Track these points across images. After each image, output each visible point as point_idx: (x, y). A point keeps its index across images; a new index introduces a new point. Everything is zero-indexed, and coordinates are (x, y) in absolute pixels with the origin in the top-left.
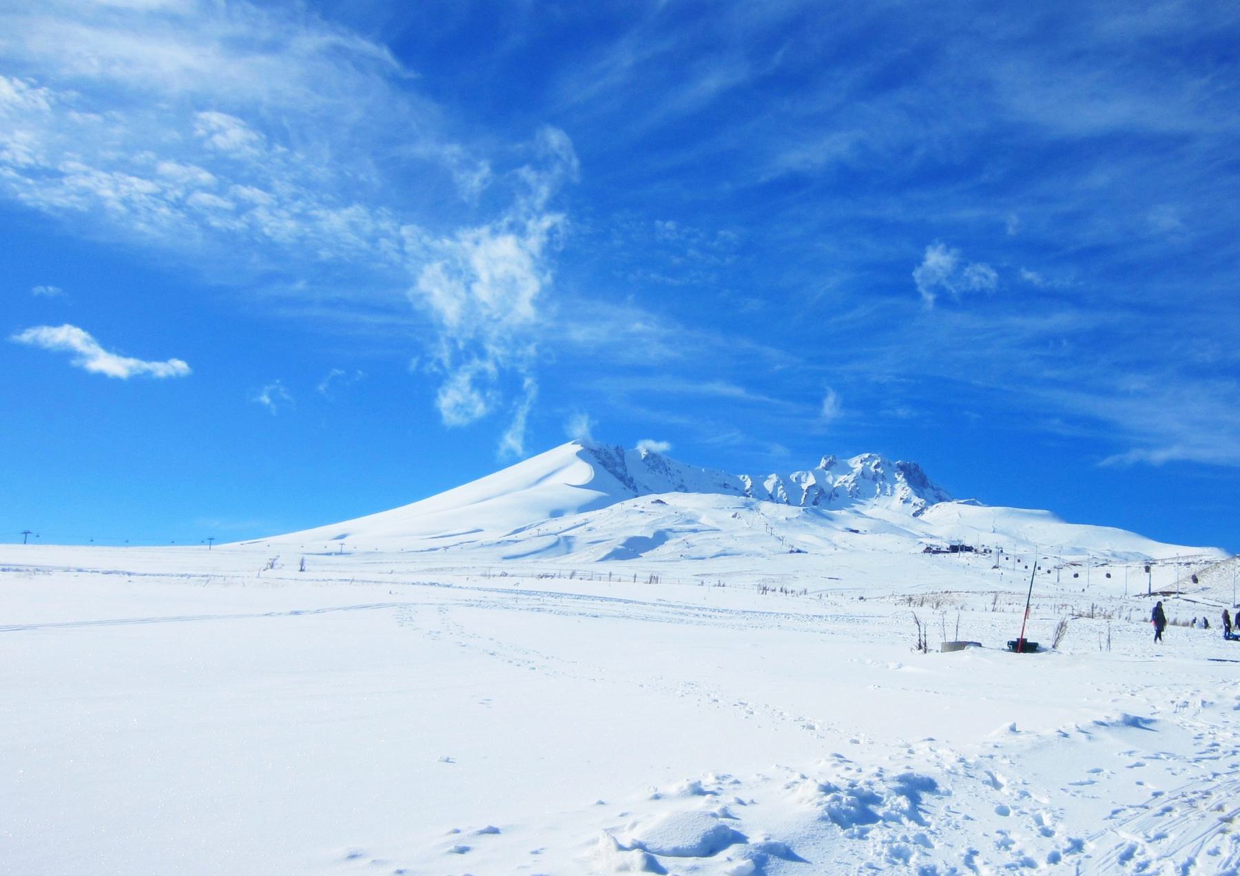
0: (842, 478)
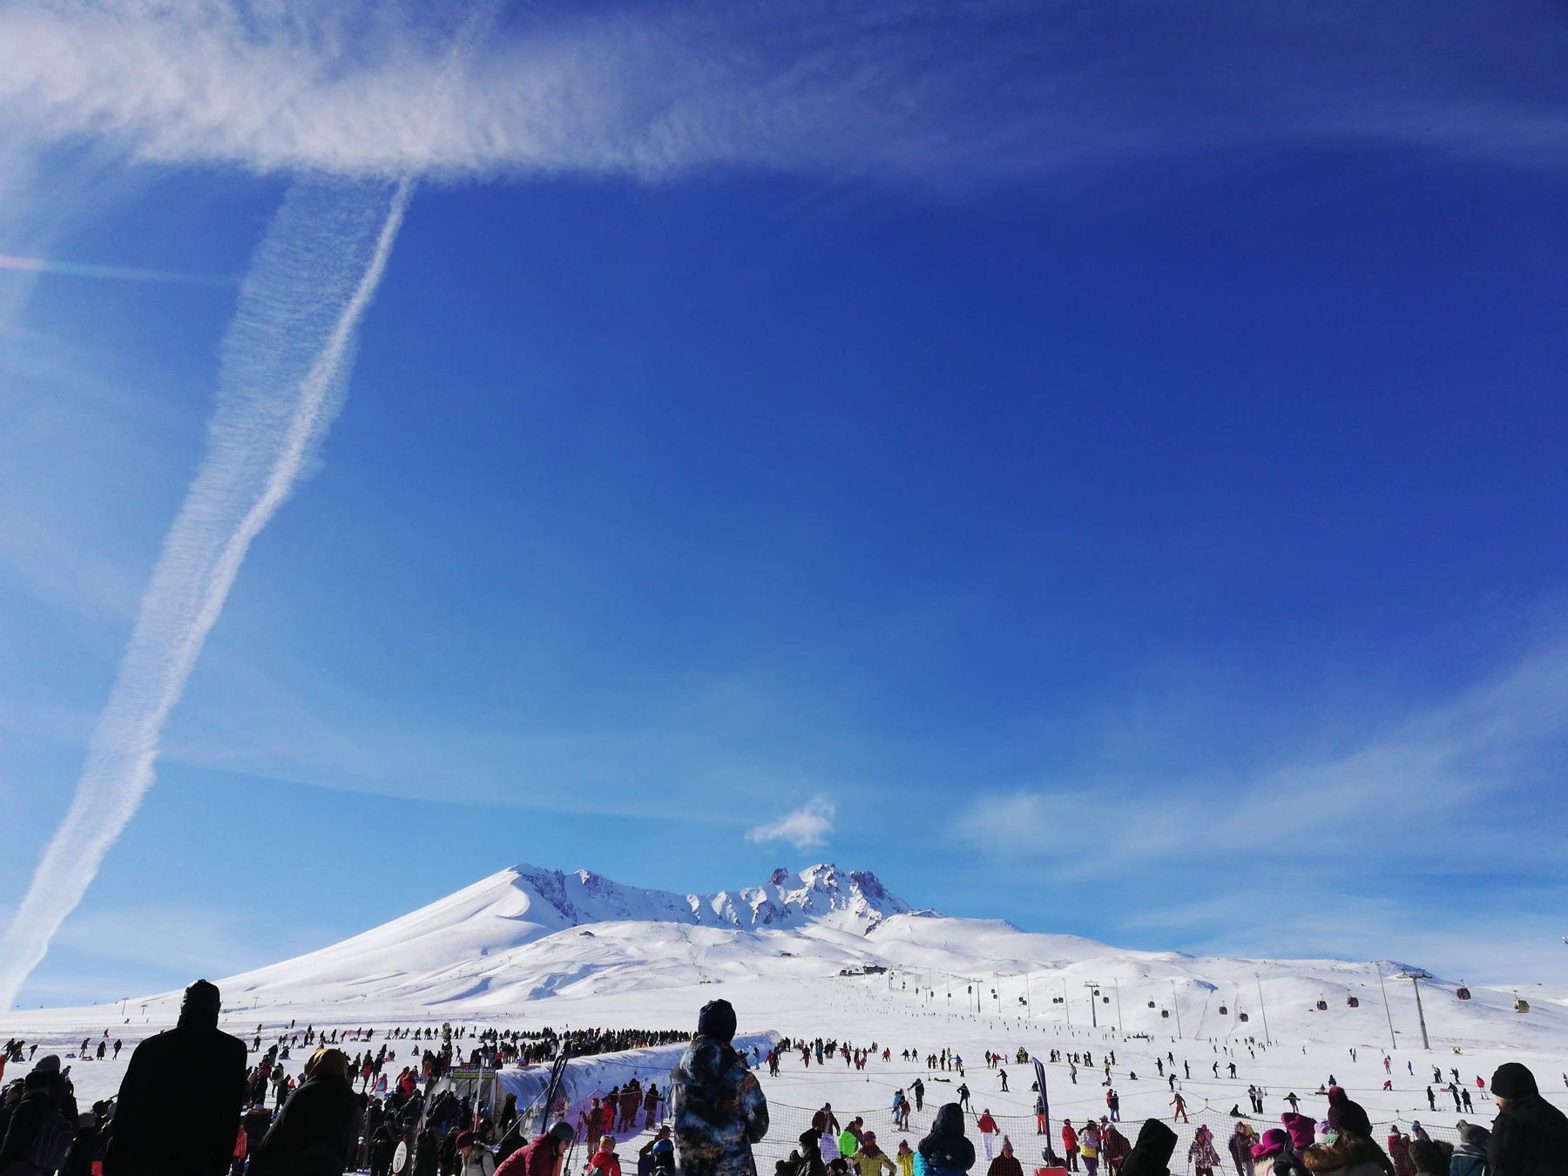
0: (794, 893)
